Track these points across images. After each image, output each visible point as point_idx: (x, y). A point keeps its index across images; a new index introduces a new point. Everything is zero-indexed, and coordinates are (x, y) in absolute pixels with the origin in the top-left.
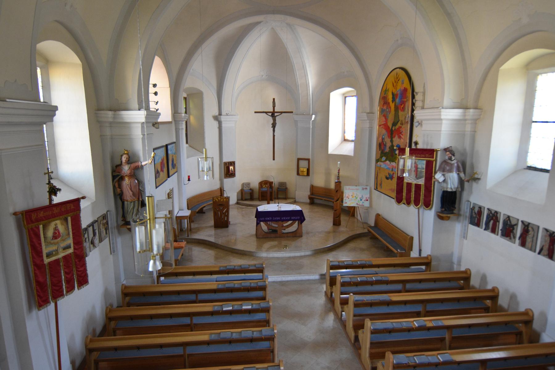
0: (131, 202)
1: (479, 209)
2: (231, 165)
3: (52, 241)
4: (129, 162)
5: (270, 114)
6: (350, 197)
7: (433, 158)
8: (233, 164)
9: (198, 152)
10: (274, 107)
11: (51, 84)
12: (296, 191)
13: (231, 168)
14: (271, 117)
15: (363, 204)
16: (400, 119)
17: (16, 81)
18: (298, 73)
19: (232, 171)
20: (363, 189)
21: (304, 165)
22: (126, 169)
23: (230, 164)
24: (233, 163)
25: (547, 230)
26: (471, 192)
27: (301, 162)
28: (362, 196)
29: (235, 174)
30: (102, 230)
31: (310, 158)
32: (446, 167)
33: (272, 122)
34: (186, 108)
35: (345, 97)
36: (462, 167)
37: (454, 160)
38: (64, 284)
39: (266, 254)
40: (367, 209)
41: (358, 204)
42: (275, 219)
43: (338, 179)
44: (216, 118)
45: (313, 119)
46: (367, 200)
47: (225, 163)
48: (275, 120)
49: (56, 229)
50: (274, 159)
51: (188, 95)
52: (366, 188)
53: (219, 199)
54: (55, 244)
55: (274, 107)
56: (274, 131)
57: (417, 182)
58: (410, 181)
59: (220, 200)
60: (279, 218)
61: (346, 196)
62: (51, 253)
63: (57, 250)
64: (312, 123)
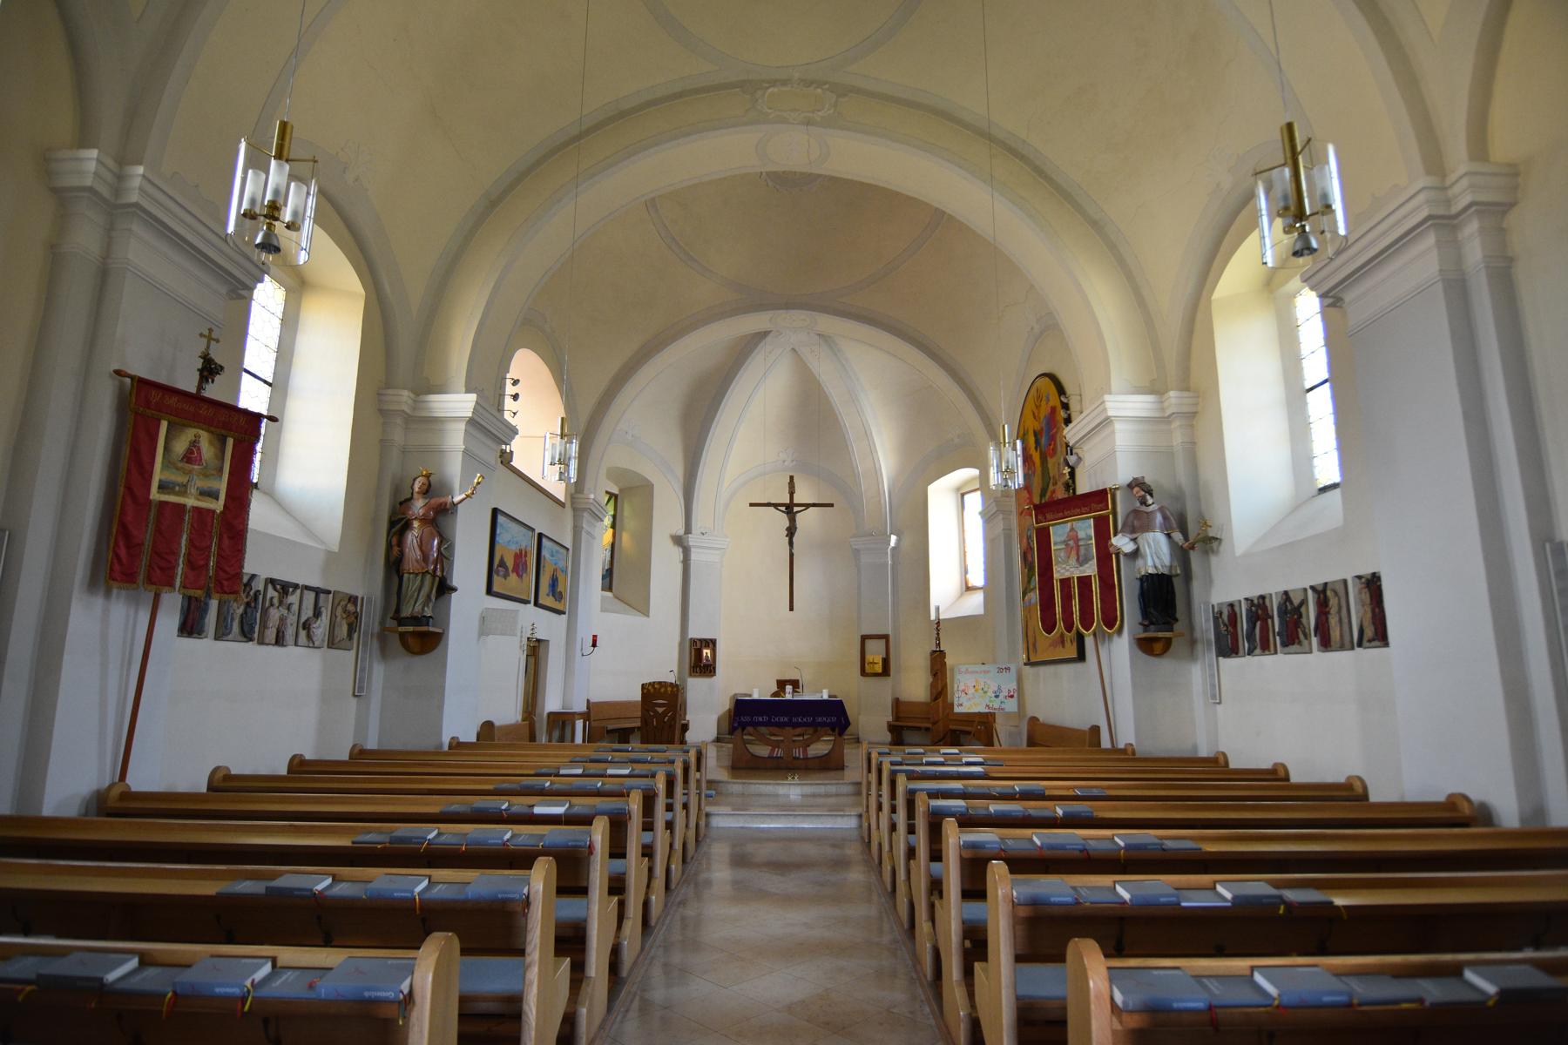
0: (417, 574)
1: (1230, 608)
2: (707, 646)
3: (180, 465)
4: (427, 491)
5: (783, 509)
6: (971, 691)
7: (1108, 509)
8: (711, 645)
9: (630, 609)
10: (792, 494)
11: (301, 322)
12: (859, 714)
14: (785, 515)
15: (1003, 706)
16: (1051, 475)
17: (197, 186)
18: (856, 448)
19: (707, 660)
20: (1000, 670)
21: (875, 653)
22: (419, 506)
23: (704, 645)
24: (711, 643)
25: (1359, 577)
26: (1209, 581)
28: (999, 688)
29: (714, 668)
30: (338, 619)
31: (890, 633)
32: (1138, 524)
33: (788, 525)
34: (614, 517)
35: (963, 495)
36: (1178, 523)
37: (1153, 503)
38: (181, 566)
39: (741, 786)
40: (1017, 726)
41: (991, 706)
42: (777, 719)
43: (938, 645)
44: (678, 541)
45: (893, 544)
46: (1012, 696)
47: (694, 641)
48: (795, 521)
49: (194, 444)
50: (791, 609)
51: (621, 490)
54: (186, 472)
55: (792, 494)
56: (791, 543)
57: (1081, 572)
58: (1067, 575)
59: (660, 689)
60: (786, 719)
61: (960, 688)
62: (171, 485)
64: (893, 556)
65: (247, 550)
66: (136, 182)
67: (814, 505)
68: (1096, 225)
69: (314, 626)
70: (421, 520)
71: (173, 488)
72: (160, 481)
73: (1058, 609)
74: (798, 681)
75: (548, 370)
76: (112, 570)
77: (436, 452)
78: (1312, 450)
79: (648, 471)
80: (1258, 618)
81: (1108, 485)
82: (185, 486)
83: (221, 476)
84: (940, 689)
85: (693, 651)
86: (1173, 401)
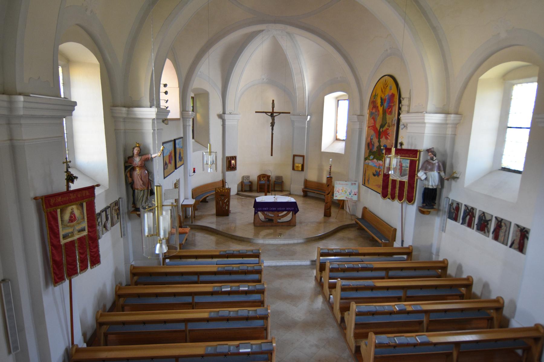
1: (457, 205)
3: (69, 224)
4: (140, 154)
5: (270, 114)
6: (340, 191)
7: (417, 158)
8: (234, 158)
10: (273, 108)
12: (291, 184)
13: (233, 162)
15: (352, 198)
17: (39, 78)
18: (296, 78)
20: (352, 184)
21: (299, 160)
22: (137, 160)
23: (232, 159)
24: (234, 158)
25: (518, 226)
26: (450, 190)
27: (296, 158)
28: (351, 191)
29: (236, 167)
32: (428, 166)
33: (271, 122)
35: (338, 101)
36: (443, 167)
37: (436, 160)
38: (78, 263)
39: (262, 241)
41: (348, 197)
43: (330, 174)
44: (220, 116)
45: (308, 120)
46: (356, 194)
47: (228, 158)
48: (274, 120)
49: (72, 213)
51: (195, 95)
52: (355, 184)
53: (221, 189)
54: (71, 226)
55: (273, 108)
56: (272, 129)
58: (395, 178)
61: (337, 190)
62: (67, 235)
63: (73, 232)
65: (100, 244)
66: (21, 105)
67: (283, 113)
68: (434, 29)
69: (107, 224)
70: (139, 167)
71: (68, 235)
72: (63, 235)
73: (389, 190)
74: (270, 176)
75: (171, 62)
76: (55, 280)
77: (140, 133)
78: (503, 153)
79: (207, 87)
80: (469, 214)
81: (418, 148)
82: (73, 232)
83: (84, 221)
84: (329, 191)
85: (228, 161)
86: (452, 118)
